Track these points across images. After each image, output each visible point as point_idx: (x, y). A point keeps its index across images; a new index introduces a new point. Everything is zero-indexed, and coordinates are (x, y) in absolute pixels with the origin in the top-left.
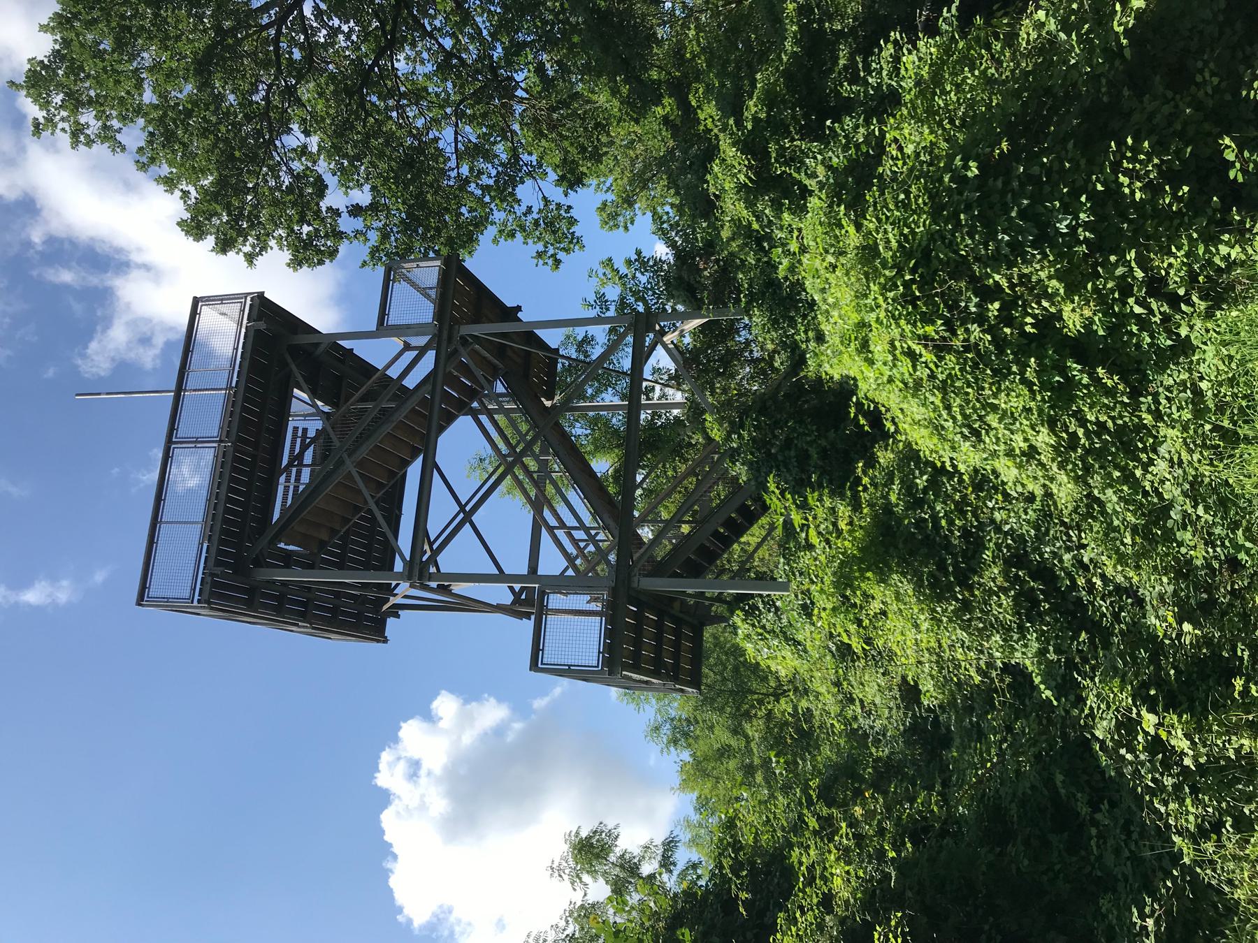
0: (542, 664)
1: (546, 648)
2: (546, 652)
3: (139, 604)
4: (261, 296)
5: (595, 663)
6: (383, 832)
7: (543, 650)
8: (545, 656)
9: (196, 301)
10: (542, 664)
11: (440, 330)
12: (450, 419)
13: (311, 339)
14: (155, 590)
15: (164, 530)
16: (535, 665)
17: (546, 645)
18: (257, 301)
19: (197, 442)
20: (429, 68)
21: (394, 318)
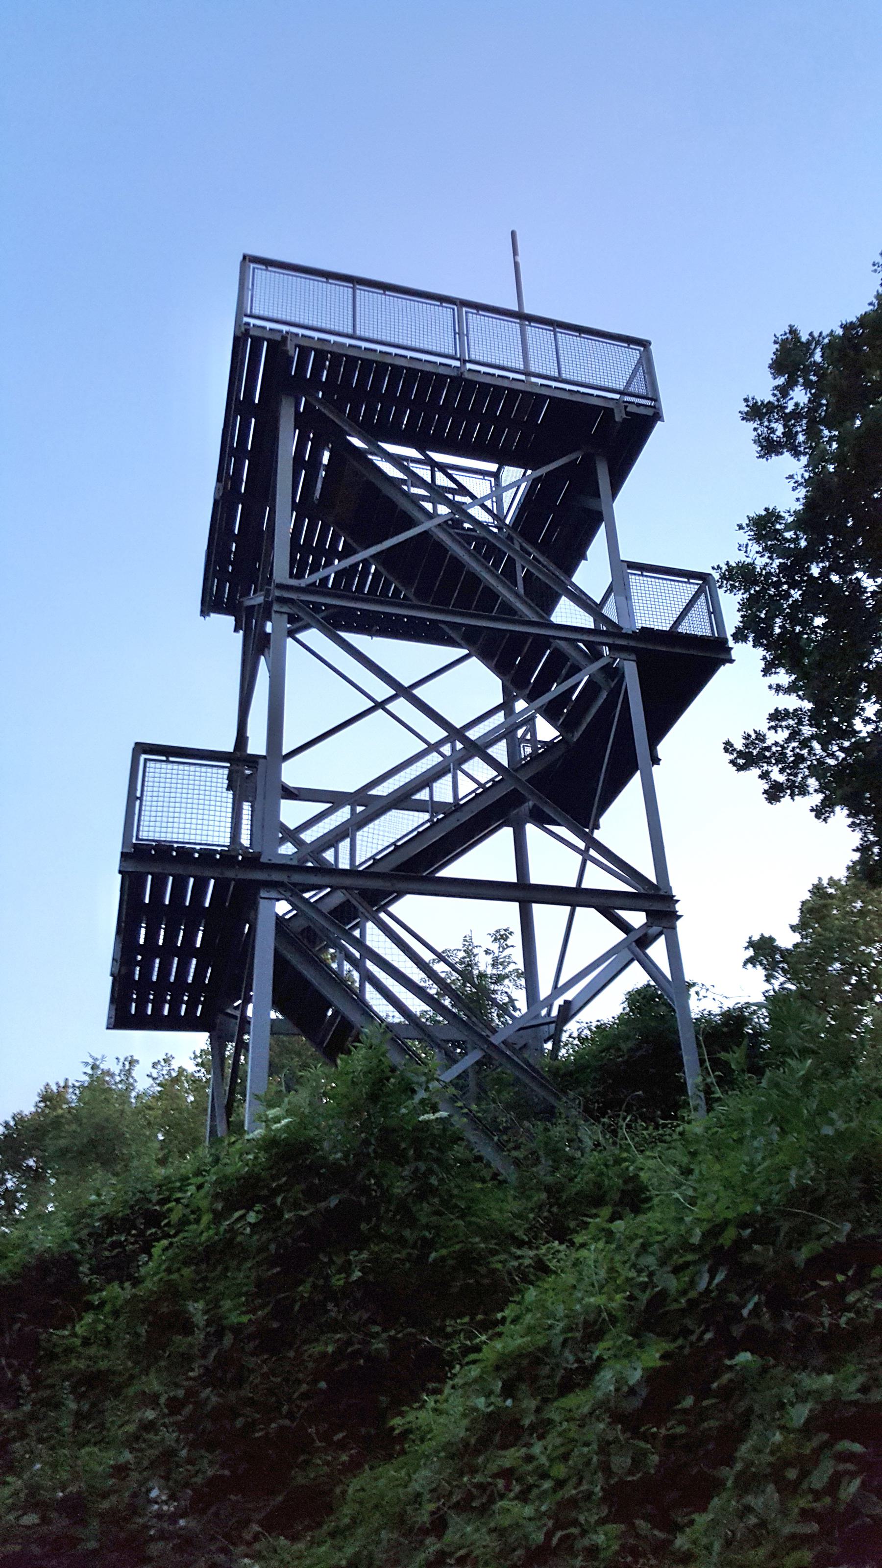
0: (146, 760)
1: (170, 766)
2: (164, 765)
3: (244, 257)
4: (657, 416)
5: (150, 765)
6: (19, 1119)
7: (167, 761)
8: (158, 765)
9: (644, 344)
10: (146, 760)
11: (626, 636)
12: (499, 669)
13: (508, 684)
14: (262, 276)
15: (344, 291)
16: (141, 748)
17: (175, 766)
18: (650, 412)
19: (460, 333)
20: (425, 1205)
21: (636, 581)
